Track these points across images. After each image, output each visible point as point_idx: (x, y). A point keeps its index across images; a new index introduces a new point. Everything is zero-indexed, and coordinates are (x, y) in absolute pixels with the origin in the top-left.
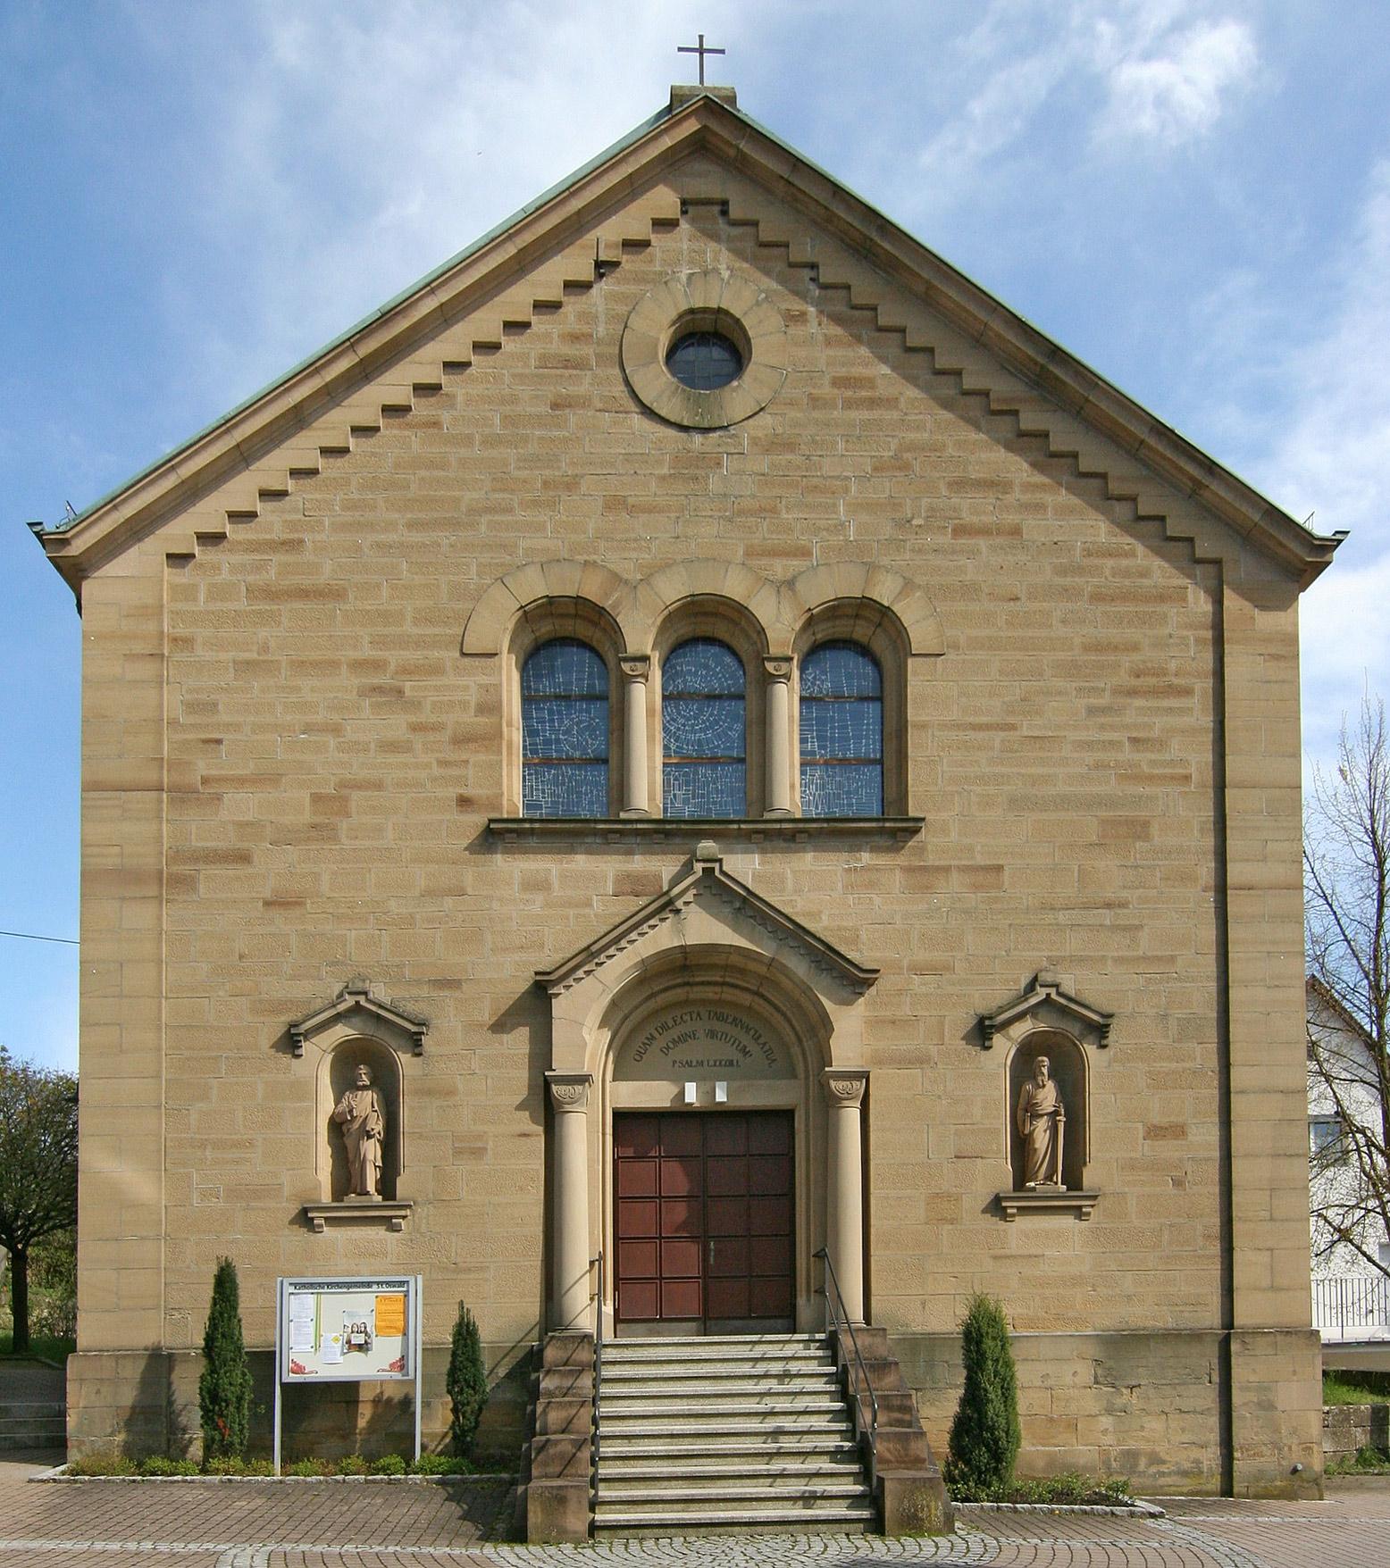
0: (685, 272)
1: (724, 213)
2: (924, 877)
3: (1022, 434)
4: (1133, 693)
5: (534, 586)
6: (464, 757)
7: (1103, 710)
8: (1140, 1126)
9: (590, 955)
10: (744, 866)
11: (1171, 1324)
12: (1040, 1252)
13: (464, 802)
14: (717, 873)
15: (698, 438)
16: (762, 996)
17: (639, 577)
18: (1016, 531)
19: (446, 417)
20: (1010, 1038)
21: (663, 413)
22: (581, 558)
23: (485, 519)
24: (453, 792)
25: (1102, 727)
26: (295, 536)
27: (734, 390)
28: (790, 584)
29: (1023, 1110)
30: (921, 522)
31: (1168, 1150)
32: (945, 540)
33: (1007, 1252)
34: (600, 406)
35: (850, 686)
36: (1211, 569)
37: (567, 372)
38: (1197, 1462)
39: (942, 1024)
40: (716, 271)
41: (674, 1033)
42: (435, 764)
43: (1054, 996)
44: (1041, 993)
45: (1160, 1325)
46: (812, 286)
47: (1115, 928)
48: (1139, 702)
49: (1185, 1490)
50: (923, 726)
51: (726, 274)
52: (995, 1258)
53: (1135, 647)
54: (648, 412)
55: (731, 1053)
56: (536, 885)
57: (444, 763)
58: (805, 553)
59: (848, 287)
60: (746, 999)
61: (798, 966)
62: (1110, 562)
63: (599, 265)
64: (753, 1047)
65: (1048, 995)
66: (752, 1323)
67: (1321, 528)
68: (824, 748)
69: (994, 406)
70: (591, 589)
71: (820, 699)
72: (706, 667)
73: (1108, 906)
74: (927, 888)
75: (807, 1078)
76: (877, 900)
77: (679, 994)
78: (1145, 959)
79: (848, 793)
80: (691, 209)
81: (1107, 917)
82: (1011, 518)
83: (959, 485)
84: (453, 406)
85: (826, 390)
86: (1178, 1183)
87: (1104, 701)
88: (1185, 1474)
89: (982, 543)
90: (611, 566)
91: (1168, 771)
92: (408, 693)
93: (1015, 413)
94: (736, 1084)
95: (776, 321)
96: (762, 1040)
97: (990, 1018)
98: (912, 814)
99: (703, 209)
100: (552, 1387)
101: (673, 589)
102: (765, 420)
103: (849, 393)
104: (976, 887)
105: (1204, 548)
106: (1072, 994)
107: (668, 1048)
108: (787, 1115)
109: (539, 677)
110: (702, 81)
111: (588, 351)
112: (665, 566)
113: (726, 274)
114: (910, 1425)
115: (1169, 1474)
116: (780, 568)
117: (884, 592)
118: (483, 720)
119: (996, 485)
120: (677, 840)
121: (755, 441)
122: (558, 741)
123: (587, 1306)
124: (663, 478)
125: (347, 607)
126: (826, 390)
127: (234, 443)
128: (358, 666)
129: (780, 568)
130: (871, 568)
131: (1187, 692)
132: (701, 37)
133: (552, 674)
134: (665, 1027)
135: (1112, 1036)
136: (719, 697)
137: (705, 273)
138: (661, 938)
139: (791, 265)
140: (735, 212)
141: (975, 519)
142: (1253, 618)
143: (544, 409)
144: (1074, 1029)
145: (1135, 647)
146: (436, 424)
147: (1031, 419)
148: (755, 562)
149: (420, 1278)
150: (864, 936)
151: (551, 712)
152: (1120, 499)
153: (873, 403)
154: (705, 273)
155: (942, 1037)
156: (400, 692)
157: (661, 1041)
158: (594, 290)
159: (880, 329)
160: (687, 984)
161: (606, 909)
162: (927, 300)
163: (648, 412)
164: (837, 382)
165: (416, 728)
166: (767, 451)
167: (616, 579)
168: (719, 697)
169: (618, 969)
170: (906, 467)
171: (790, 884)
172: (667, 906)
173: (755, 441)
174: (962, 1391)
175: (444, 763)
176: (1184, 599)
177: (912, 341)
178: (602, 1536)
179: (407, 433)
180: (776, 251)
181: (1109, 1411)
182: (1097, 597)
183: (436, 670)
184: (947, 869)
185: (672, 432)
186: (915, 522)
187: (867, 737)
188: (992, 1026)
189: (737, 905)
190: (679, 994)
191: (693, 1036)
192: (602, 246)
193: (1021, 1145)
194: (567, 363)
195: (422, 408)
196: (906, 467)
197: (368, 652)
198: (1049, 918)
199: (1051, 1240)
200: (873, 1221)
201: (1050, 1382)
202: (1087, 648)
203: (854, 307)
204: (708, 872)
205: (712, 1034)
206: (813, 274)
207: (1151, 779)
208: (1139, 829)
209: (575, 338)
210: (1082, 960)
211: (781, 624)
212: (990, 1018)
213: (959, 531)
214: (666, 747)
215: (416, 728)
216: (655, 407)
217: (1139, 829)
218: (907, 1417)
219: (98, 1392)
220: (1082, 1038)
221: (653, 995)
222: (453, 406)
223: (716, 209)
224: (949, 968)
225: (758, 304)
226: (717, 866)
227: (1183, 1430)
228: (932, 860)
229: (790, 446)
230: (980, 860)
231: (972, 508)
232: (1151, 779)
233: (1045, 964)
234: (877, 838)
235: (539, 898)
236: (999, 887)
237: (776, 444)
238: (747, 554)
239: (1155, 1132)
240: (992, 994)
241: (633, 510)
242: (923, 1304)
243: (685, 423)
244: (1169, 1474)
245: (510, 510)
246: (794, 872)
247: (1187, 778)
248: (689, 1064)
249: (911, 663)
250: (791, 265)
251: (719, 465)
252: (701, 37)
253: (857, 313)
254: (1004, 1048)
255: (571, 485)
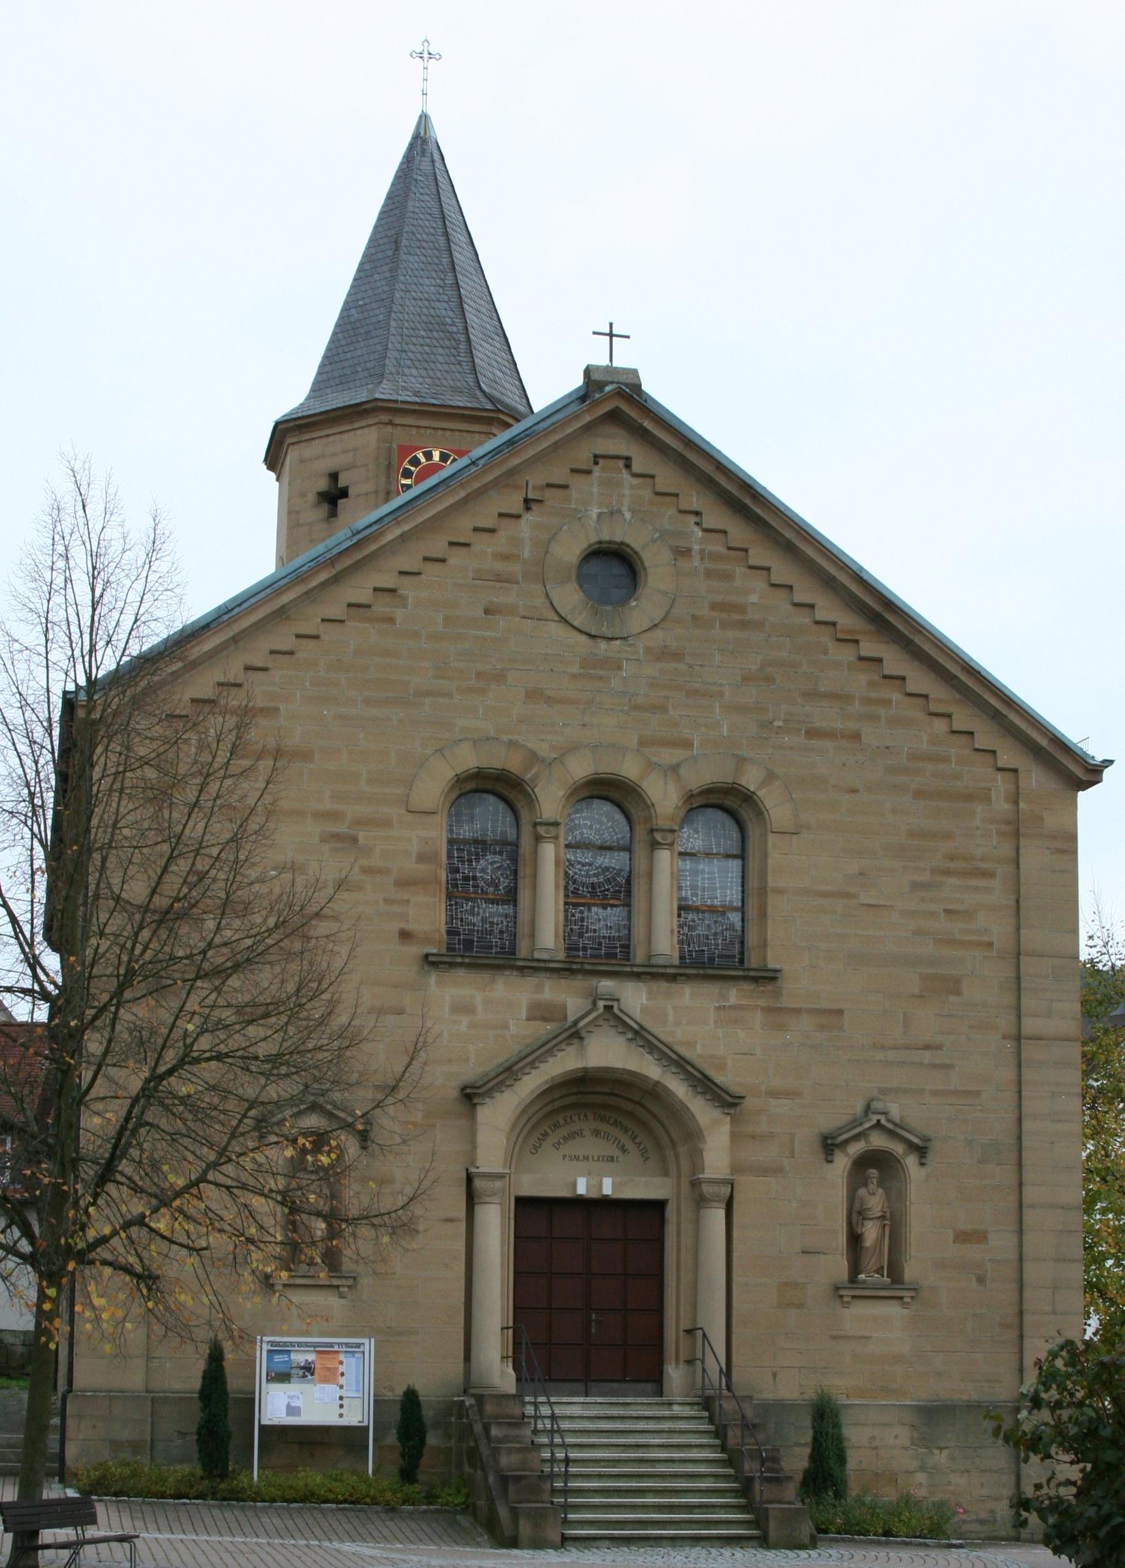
0: (594, 512)
1: (628, 466)
2: (778, 1015)
3: (861, 659)
4: (948, 873)
5: (468, 760)
6: (406, 897)
7: (924, 886)
8: (950, 1231)
9: (509, 1073)
10: (635, 998)
11: (975, 1397)
12: (868, 1334)
13: (405, 935)
14: (616, 1010)
15: (603, 645)
16: (642, 1106)
17: (553, 755)
18: (856, 736)
19: (399, 614)
20: (847, 1155)
21: (576, 623)
22: (506, 738)
23: (427, 701)
24: (396, 926)
25: (923, 900)
26: (272, 704)
27: (633, 608)
28: (675, 769)
29: (856, 1215)
30: (780, 724)
31: (972, 1252)
32: (800, 740)
33: (843, 1333)
34: (523, 613)
35: (718, 845)
36: (1010, 775)
37: (498, 585)
38: (992, 1511)
39: (792, 1140)
40: (619, 512)
41: (564, 1131)
42: (382, 902)
43: (883, 1122)
44: (874, 1119)
45: (965, 1397)
46: (696, 529)
47: (934, 1066)
48: (952, 881)
49: (982, 1536)
50: (780, 891)
51: (628, 516)
52: (834, 1338)
53: (949, 836)
54: (564, 620)
55: (614, 1151)
56: (463, 1008)
57: (387, 901)
58: (688, 744)
59: (725, 532)
60: (630, 1106)
61: (678, 1088)
62: (930, 766)
63: (527, 501)
64: (630, 1145)
65: (879, 1121)
66: (625, 1386)
67: (1096, 752)
68: (696, 895)
69: (840, 636)
70: (513, 763)
71: (694, 855)
72: (601, 823)
73: (927, 1047)
74: (781, 1027)
75: (679, 1177)
76: (742, 1034)
77: (573, 1099)
78: (955, 1093)
79: (715, 934)
80: (601, 461)
81: (927, 1057)
82: (851, 725)
83: (812, 695)
84: (405, 606)
85: (705, 612)
86: (981, 1280)
87: (925, 877)
88: (982, 1522)
89: (829, 744)
90: (529, 745)
91: (974, 938)
92: (361, 841)
93: (857, 642)
94: (618, 1179)
95: (666, 555)
96: (637, 1141)
97: (833, 1138)
98: (771, 966)
99: (611, 462)
100: (500, 1436)
101: (581, 768)
102: (659, 634)
103: (725, 616)
104: (822, 1027)
105: (1004, 760)
106: (898, 1120)
107: (559, 1143)
108: (659, 1206)
109: (459, 822)
110: (611, 360)
111: (515, 568)
112: (574, 748)
113: (628, 516)
114: (777, 1471)
115: (971, 1522)
116: (669, 756)
117: (750, 780)
118: (422, 867)
119: (840, 697)
120: (580, 977)
121: (648, 650)
122: (475, 878)
123: (497, 1370)
124: (574, 676)
125: (313, 766)
126: (705, 612)
127: (231, 634)
128: (320, 816)
129: (669, 756)
130: (741, 761)
131: (989, 875)
132: (611, 325)
133: (472, 819)
134: (557, 1126)
135: (930, 1156)
136: (610, 848)
137: (612, 513)
138: (566, 1062)
139: (681, 512)
140: (636, 467)
141: (824, 724)
142: (1042, 819)
143: (480, 612)
144: (898, 1149)
145: (949, 836)
146: (391, 620)
147: (869, 648)
148: (646, 750)
149: (373, 1340)
150: (729, 1062)
151: (470, 853)
152: (937, 715)
153: (744, 625)
154: (612, 513)
155: (793, 1151)
156: (354, 840)
157: (553, 1138)
158: (523, 521)
159: (751, 567)
160: (581, 1093)
161: (521, 1031)
162: (789, 549)
163: (564, 620)
164: (714, 606)
165: (366, 871)
166: (658, 659)
167: (533, 757)
168: (610, 848)
169: (532, 1083)
170: (769, 679)
171: (671, 1019)
172: (575, 1035)
173: (648, 650)
174: (808, 1451)
175: (387, 901)
176: (989, 799)
177: (776, 579)
178: (567, 1543)
179: (366, 625)
180: (668, 499)
181: (923, 1468)
182: (919, 794)
183: (386, 823)
184: (798, 1011)
185: (584, 638)
186: (776, 724)
187: (731, 889)
188: (833, 1145)
189: (630, 1036)
190: (573, 1099)
191: (580, 1134)
192: (530, 487)
193: (855, 1240)
194: (500, 578)
195: (381, 608)
196: (769, 679)
197: (328, 805)
198: (880, 1056)
199: (882, 1325)
200: (735, 1303)
201: (876, 1443)
202: (912, 834)
203: (729, 548)
204: (609, 1008)
205: (596, 1133)
206: (697, 519)
207: (962, 944)
208: (953, 986)
209: (506, 558)
210: (906, 1091)
211: (664, 797)
212: (833, 1138)
213: (811, 733)
214: (566, 888)
215: (366, 871)
216: (569, 618)
217: (953, 986)
218: (776, 1466)
219: (94, 1427)
220: (906, 1155)
221: (552, 1101)
222: (405, 606)
223: (621, 463)
224: (799, 1094)
225: (653, 541)
226: (615, 1004)
227: (982, 1485)
228: (786, 1002)
229: (677, 656)
230: (826, 1005)
231: (825, 716)
232: (962, 944)
233: (876, 1093)
234: (742, 982)
235: (465, 1020)
236: (841, 1028)
237: (664, 654)
238: (642, 743)
239: (963, 1237)
240: (830, 1119)
241: (549, 701)
242: (774, 1375)
243: (593, 633)
244: (971, 1522)
245: (449, 695)
246: (674, 1008)
247: (990, 945)
248: (577, 1158)
249: (771, 839)
250: (681, 512)
251: (620, 668)
252: (611, 325)
253: (731, 553)
254: (842, 1162)
255: (499, 677)
